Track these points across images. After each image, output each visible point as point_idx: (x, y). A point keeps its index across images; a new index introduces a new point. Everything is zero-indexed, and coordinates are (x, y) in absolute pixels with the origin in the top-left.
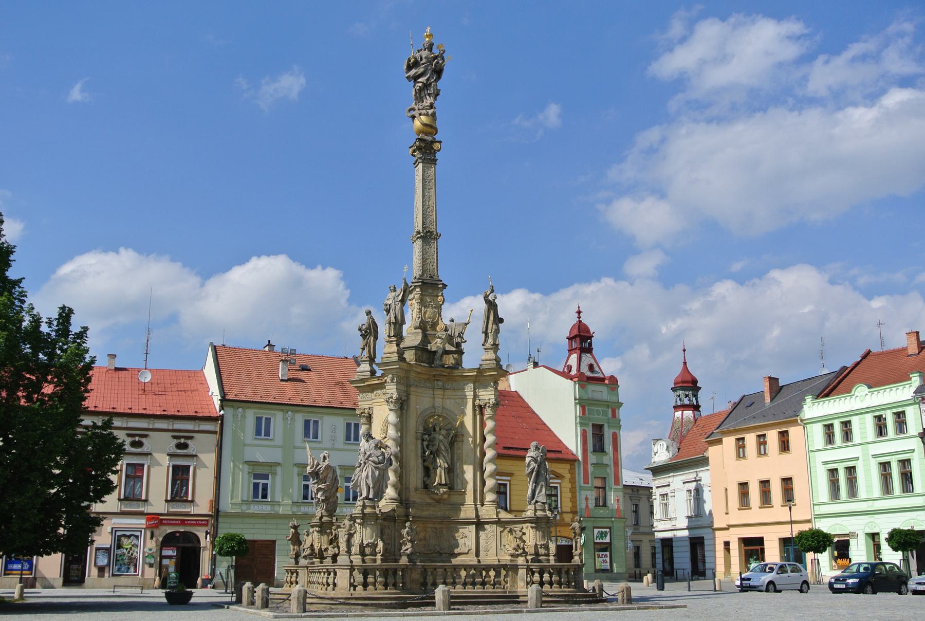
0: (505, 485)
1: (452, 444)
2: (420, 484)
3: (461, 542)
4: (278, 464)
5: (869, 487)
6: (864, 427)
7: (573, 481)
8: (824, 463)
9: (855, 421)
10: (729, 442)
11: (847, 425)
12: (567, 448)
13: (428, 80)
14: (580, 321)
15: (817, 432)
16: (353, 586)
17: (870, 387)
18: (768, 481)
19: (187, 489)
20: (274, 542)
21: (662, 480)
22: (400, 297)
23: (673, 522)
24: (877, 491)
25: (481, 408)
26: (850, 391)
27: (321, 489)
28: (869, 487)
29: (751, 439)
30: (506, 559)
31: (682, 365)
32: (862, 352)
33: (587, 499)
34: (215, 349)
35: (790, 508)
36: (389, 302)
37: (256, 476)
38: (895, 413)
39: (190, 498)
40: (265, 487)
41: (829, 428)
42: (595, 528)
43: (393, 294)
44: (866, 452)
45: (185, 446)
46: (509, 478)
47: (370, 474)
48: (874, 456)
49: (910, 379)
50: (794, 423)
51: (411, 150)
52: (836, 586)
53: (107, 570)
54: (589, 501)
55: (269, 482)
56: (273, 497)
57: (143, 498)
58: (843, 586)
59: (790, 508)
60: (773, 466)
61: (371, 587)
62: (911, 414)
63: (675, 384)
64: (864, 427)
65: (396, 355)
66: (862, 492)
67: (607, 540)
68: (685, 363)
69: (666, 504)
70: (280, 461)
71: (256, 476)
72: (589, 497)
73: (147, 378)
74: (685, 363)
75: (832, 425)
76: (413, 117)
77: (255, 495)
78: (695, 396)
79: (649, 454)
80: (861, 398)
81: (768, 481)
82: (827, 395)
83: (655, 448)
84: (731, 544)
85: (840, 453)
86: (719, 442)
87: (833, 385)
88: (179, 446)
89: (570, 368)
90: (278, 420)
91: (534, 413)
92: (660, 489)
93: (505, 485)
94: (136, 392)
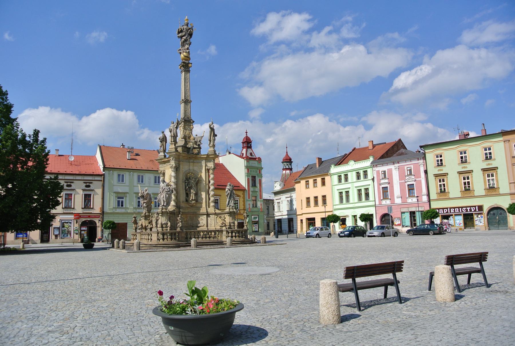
4: (128, 193)
8: (338, 190)
9: (349, 174)
10: (303, 182)
11: (346, 176)
15: (335, 178)
16: (158, 239)
20: (127, 223)
21: (278, 197)
29: (311, 181)
30: (218, 228)
34: (100, 147)
37: (119, 198)
40: (122, 202)
41: (340, 177)
44: (353, 186)
45: (89, 186)
50: (327, 175)
60: (319, 191)
61: (165, 240)
62: (369, 171)
64: (352, 176)
66: (351, 200)
71: (119, 198)
73: (72, 159)
76: (181, 53)
77: (119, 205)
78: (291, 165)
79: (273, 187)
80: (352, 165)
82: (339, 164)
85: (344, 186)
86: (300, 182)
89: (243, 154)
90: (127, 175)
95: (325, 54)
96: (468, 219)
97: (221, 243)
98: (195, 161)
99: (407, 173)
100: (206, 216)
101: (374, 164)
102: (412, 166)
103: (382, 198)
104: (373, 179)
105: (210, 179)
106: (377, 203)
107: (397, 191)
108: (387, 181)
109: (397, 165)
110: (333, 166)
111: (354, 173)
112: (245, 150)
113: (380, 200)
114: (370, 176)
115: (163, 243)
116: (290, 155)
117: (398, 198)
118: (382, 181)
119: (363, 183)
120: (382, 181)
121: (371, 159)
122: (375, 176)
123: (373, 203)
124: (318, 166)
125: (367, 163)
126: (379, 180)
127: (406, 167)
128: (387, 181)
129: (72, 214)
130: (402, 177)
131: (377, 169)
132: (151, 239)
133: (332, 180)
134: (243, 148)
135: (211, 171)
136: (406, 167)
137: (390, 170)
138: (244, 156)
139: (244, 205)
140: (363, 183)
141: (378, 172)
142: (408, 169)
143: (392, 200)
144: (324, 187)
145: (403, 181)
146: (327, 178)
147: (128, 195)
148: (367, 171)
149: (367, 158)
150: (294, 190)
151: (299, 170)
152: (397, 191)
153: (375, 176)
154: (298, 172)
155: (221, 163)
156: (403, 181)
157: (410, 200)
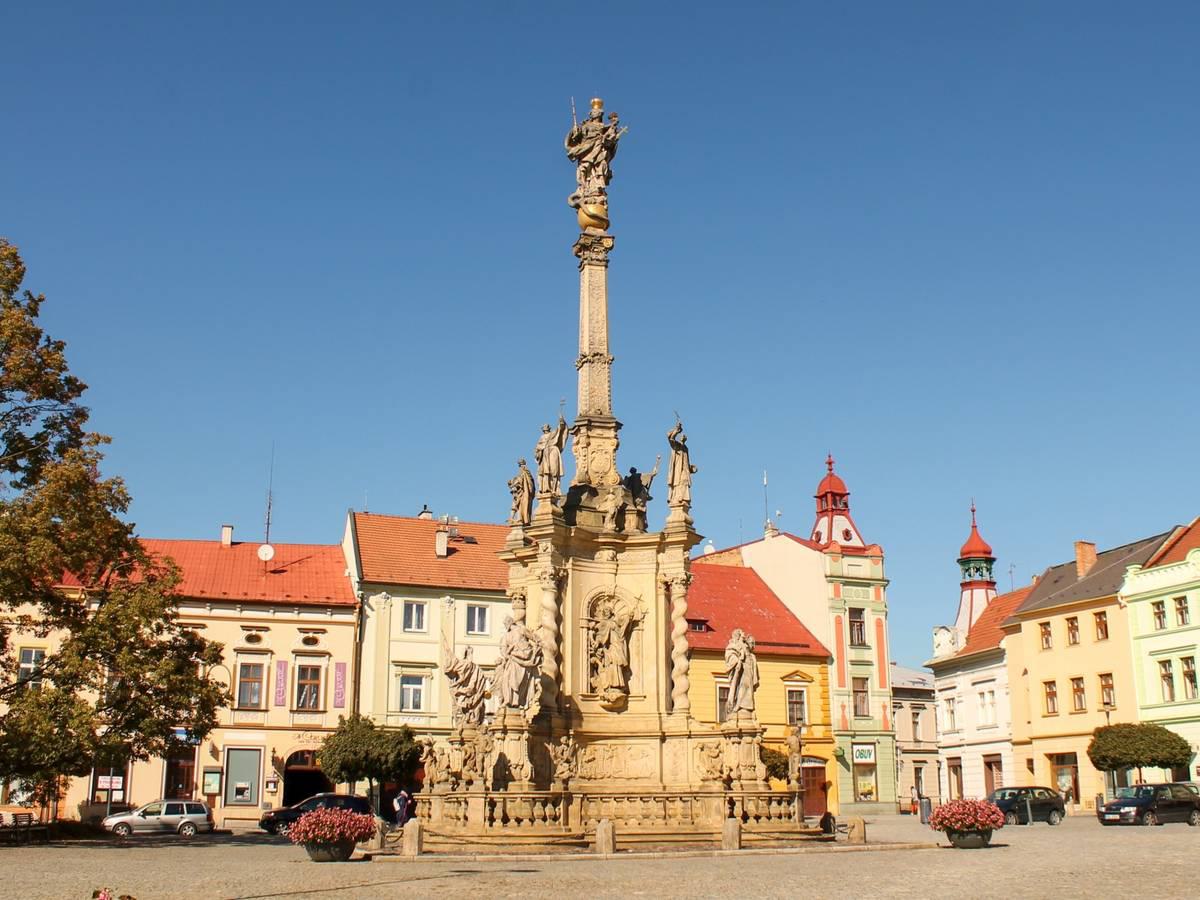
1: (628, 635)
7: (825, 684)
8: (1152, 654)
10: (1031, 627)
11: (1181, 600)
12: (817, 641)
13: (595, 158)
14: (831, 475)
19: (317, 698)
21: (945, 682)
22: (556, 440)
23: (960, 736)
25: (668, 586)
26: (1184, 559)
29: (1058, 623)
30: (697, 785)
31: (970, 530)
33: (843, 707)
34: (354, 516)
35: (1108, 714)
36: (542, 447)
39: (321, 708)
41: (1159, 605)
42: (853, 744)
43: (547, 436)
45: (314, 641)
47: (513, 672)
50: (1114, 601)
51: (575, 249)
52: (1108, 817)
53: (218, 798)
54: (847, 710)
57: (263, 707)
58: (1117, 817)
59: (1108, 714)
60: (1087, 657)
63: (962, 554)
65: (551, 516)
67: (871, 760)
68: (974, 527)
69: (952, 712)
71: (406, 679)
72: (846, 704)
73: (266, 553)
74: (974, 527)
76: (578, 206)
78: (989, 570)
79: (930, 646)
82: (1156, 563)
83: (937, 639)
84: (1035, 762)
86: (1017, 629)
88: (250, 639)
89: (818, 535)
90: (434, 607)
91: (775, 596)
92: (944, 692)
94: (256, 573)
96: (532, 820)
97: (700, 841)
100: (658, 741)
105: (673, 615)
110: (1132, 570)
112: (825, 521)
115: (518, 832)
116: (988, 538)
129: (318, 729)
132: (466, 818)
133: (1132, 618)
134: (822, 513)
135: (678, 590)
138: (824, 541)
139: (826, 710)
146: (1111, 611)
150: (998, 656)
151: (1018, 587)
154: (1013, 594)
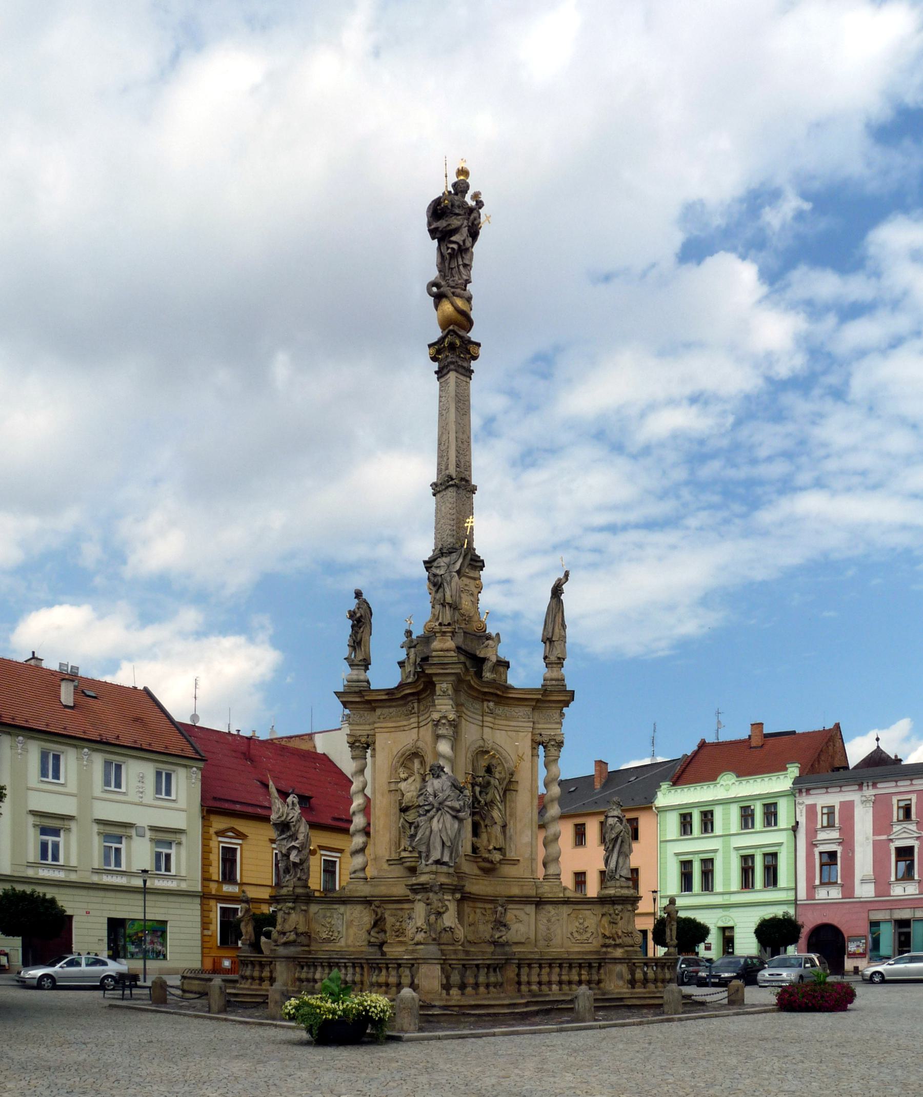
0: (335, 862)
1: (506, 791)
2: (469, 850)
3: (514, 927)
4: (71, 818)
5: (727, 881)
6: (727, 820)
8: (677, 854)
9: (718, 813)
15: (672, 822)
16: (447, 987)
17: (738, 777)
18: (584, 874)
20: (166, 922)
24: (735, 881)
27: (294, 847)
28: (727, 881)
32: (698, 742)
37: (44, 831)
38: (701, 812)
40: (56, 846)
44: (727, 845)
46: (339, 855)
48: (737, 849)
49: (786, 769)
55: (61, 840)
56: (67, 857)
61: (469, 990)
62: (784, 809)
64: (727, 820)
66: (718, 886)
70: (73, 813)
75: (690, 815)
77: (44, 856)
80: (729, 788)
81: (584, 874)
85: (697, 845)
87: (684, 772)
93: (335, 862)
95: (441, 549)
98: (500, 710)
99: (896, 814)
101: (801, 786)
102: (914, 798)
103: (817, 882)
104: (795, 829)
106: (802, 894)
107: (864, 861)
108: (835, 834)
109: (869, 792)
110: (665, 786)
111: (735, 812)
113: (811, 888)
114: (784, 820)
117: (863, 881)
118: (822, 836)
119: (760, 839)
120: (822, 836)
121: (793, 771)
122: (802, 820)
123: (790, 896)
124: (598, 786)
125: (781, 783)
126: (812, 832)
127: (895, 801)
128: (835, 834)
130: (881, 825)
131: (809, 800)
136: (895, 801)
137: (848, 808)
140: (760, 839)
141: (811, 810)
142: (902, 804)
143: (848, 888)
144: (580, 850)
145: (884, 837)
147: (73, 825)
148: (711, 812)
149: (781, 768)
152: (864, 861)
153: (802, 820)
155: (320, 750)
156: (884, 837)
157: (898, 891)
